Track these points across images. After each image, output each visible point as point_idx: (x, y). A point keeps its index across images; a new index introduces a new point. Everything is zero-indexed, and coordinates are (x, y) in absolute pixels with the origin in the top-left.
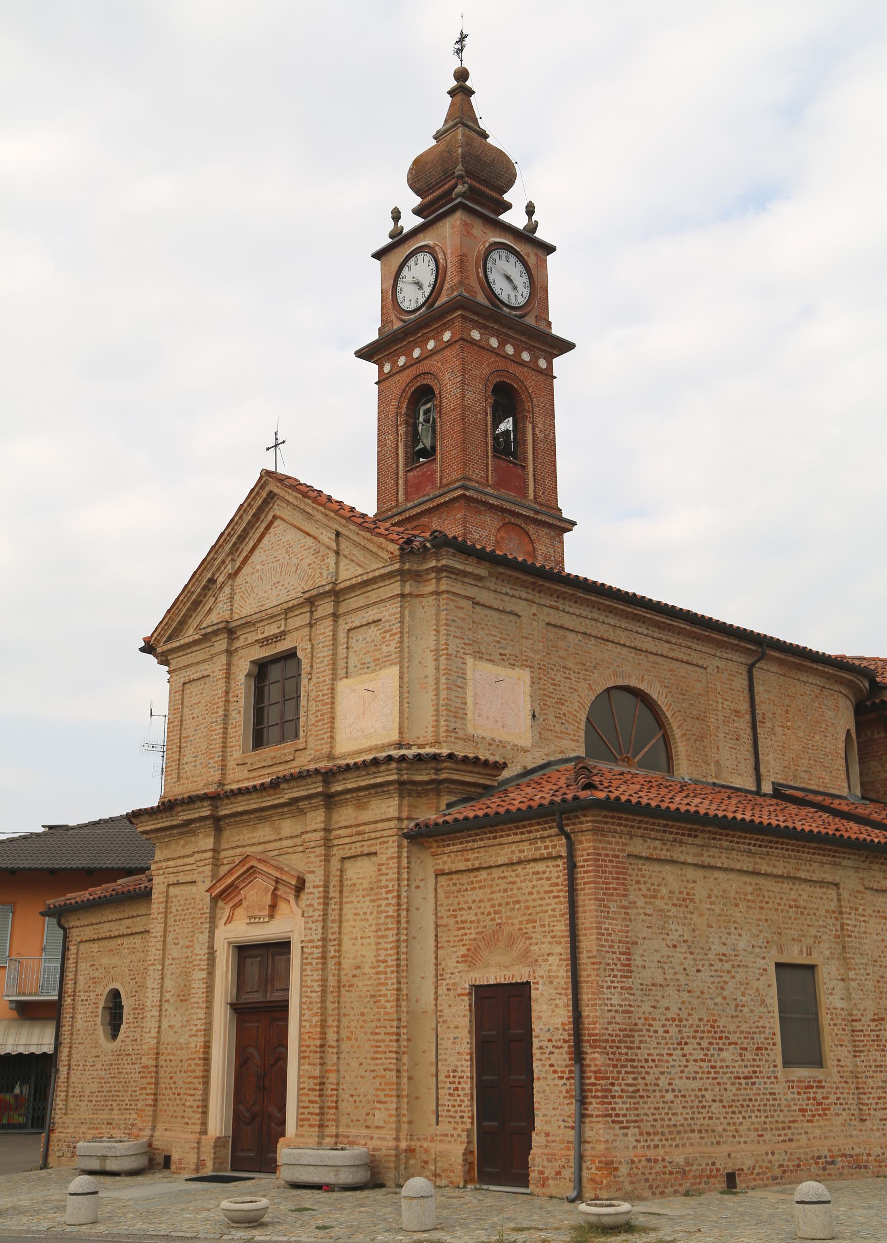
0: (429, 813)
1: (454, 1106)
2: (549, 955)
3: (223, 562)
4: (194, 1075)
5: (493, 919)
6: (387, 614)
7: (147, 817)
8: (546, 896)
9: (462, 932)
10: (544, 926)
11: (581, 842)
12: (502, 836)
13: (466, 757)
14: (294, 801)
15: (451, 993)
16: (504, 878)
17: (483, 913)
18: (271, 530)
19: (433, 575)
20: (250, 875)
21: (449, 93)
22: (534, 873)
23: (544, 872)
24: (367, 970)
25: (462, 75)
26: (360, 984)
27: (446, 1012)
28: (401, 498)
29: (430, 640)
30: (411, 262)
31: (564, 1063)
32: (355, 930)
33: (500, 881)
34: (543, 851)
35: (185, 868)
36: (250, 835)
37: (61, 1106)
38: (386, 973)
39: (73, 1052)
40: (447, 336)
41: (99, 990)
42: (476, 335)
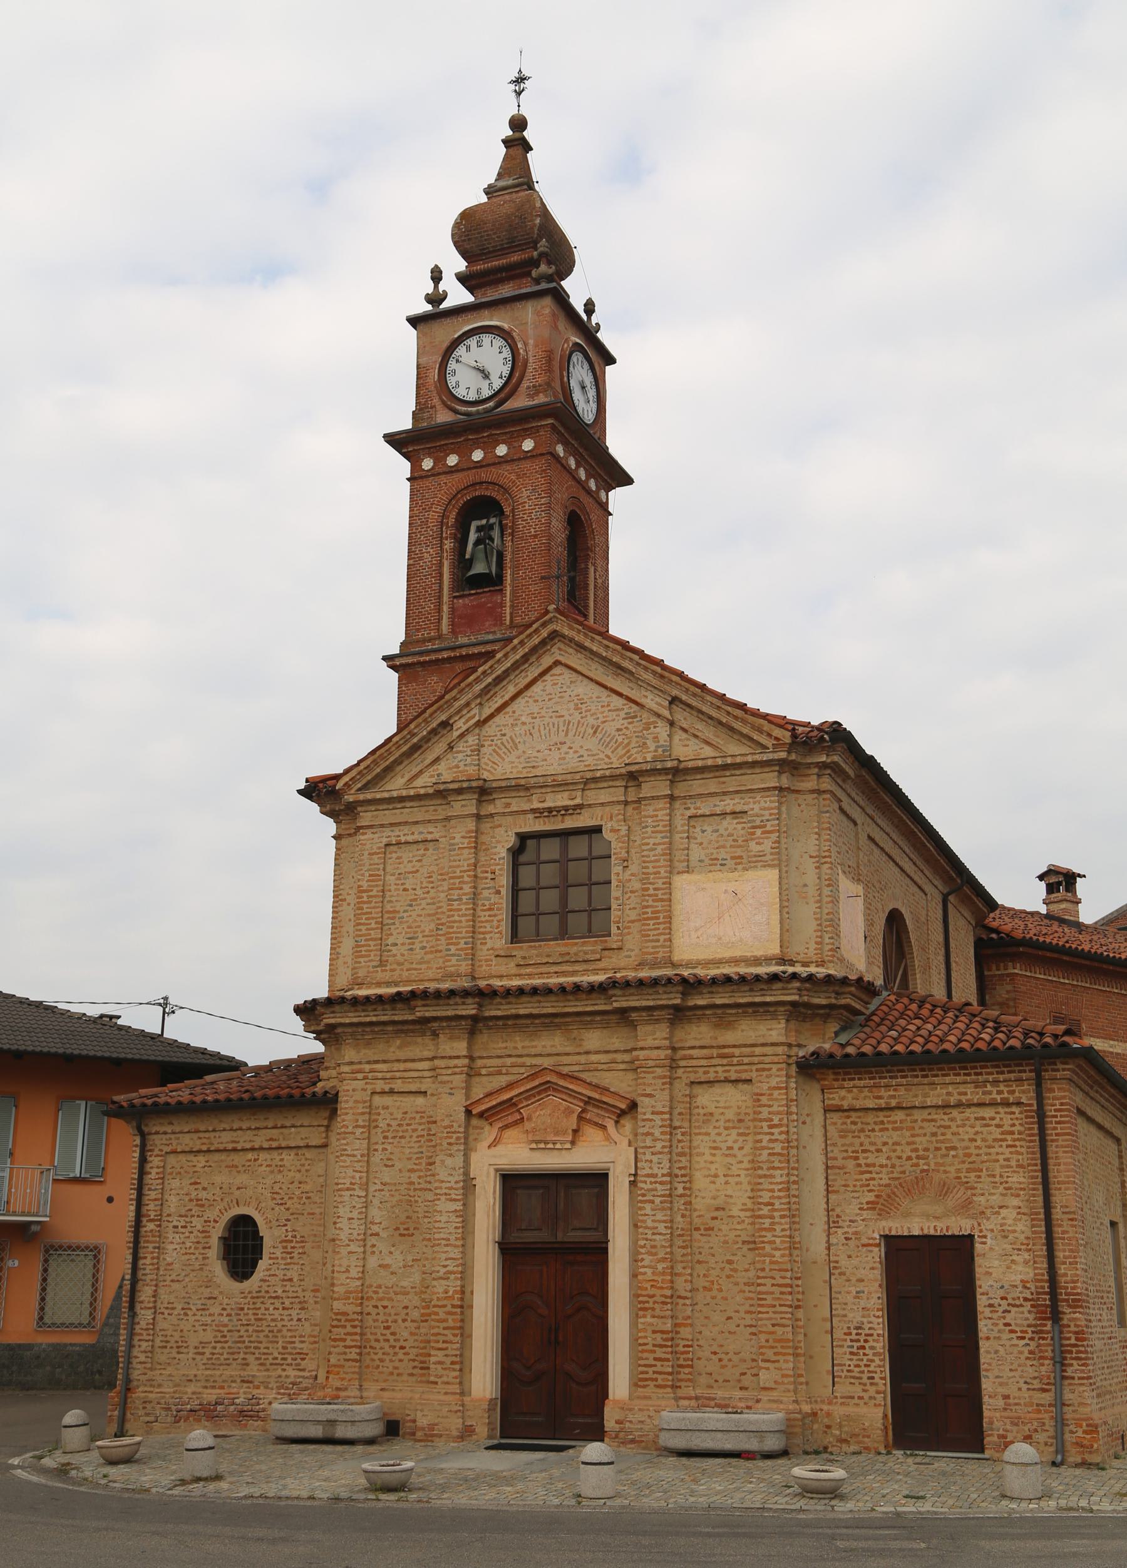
0: (822, 1041)
2: (1001, 1207)
3: (468, 704)
4: (445, 1325)
5: (917, 1165)
6: (756, 807)
8: (996, 1144)
9: (868, 1176)
10: (994, 1176)
11: (1052, 1090)
12: (937, 1076)
13: (846, 978)
14: (623, 1012)
15: (852, 1243)
16: (933, 1120)
17: (900, 1158)
18: (547, 677)
19: (816, 770)
20: (539, 1093)
21: (504, 141)
22: (976, 1119)
23: (993, 1119)
24: (735, 1212)
25: (518, 124)
26: (724, 1227)
27: (844, 1262)
29: (811, 844)
30: (472, 342)
31: (1025, 1323)
32: (713, 1167)
33: (926, 1124)
34: (994, 1096)
35: (406, 1075)
36: (527, 1043)
37: (142, 1358)
38: (772, 1217)
39: (161, 1291)
40: (528, 445)
41: (211, 1214)
42: (560, 450)
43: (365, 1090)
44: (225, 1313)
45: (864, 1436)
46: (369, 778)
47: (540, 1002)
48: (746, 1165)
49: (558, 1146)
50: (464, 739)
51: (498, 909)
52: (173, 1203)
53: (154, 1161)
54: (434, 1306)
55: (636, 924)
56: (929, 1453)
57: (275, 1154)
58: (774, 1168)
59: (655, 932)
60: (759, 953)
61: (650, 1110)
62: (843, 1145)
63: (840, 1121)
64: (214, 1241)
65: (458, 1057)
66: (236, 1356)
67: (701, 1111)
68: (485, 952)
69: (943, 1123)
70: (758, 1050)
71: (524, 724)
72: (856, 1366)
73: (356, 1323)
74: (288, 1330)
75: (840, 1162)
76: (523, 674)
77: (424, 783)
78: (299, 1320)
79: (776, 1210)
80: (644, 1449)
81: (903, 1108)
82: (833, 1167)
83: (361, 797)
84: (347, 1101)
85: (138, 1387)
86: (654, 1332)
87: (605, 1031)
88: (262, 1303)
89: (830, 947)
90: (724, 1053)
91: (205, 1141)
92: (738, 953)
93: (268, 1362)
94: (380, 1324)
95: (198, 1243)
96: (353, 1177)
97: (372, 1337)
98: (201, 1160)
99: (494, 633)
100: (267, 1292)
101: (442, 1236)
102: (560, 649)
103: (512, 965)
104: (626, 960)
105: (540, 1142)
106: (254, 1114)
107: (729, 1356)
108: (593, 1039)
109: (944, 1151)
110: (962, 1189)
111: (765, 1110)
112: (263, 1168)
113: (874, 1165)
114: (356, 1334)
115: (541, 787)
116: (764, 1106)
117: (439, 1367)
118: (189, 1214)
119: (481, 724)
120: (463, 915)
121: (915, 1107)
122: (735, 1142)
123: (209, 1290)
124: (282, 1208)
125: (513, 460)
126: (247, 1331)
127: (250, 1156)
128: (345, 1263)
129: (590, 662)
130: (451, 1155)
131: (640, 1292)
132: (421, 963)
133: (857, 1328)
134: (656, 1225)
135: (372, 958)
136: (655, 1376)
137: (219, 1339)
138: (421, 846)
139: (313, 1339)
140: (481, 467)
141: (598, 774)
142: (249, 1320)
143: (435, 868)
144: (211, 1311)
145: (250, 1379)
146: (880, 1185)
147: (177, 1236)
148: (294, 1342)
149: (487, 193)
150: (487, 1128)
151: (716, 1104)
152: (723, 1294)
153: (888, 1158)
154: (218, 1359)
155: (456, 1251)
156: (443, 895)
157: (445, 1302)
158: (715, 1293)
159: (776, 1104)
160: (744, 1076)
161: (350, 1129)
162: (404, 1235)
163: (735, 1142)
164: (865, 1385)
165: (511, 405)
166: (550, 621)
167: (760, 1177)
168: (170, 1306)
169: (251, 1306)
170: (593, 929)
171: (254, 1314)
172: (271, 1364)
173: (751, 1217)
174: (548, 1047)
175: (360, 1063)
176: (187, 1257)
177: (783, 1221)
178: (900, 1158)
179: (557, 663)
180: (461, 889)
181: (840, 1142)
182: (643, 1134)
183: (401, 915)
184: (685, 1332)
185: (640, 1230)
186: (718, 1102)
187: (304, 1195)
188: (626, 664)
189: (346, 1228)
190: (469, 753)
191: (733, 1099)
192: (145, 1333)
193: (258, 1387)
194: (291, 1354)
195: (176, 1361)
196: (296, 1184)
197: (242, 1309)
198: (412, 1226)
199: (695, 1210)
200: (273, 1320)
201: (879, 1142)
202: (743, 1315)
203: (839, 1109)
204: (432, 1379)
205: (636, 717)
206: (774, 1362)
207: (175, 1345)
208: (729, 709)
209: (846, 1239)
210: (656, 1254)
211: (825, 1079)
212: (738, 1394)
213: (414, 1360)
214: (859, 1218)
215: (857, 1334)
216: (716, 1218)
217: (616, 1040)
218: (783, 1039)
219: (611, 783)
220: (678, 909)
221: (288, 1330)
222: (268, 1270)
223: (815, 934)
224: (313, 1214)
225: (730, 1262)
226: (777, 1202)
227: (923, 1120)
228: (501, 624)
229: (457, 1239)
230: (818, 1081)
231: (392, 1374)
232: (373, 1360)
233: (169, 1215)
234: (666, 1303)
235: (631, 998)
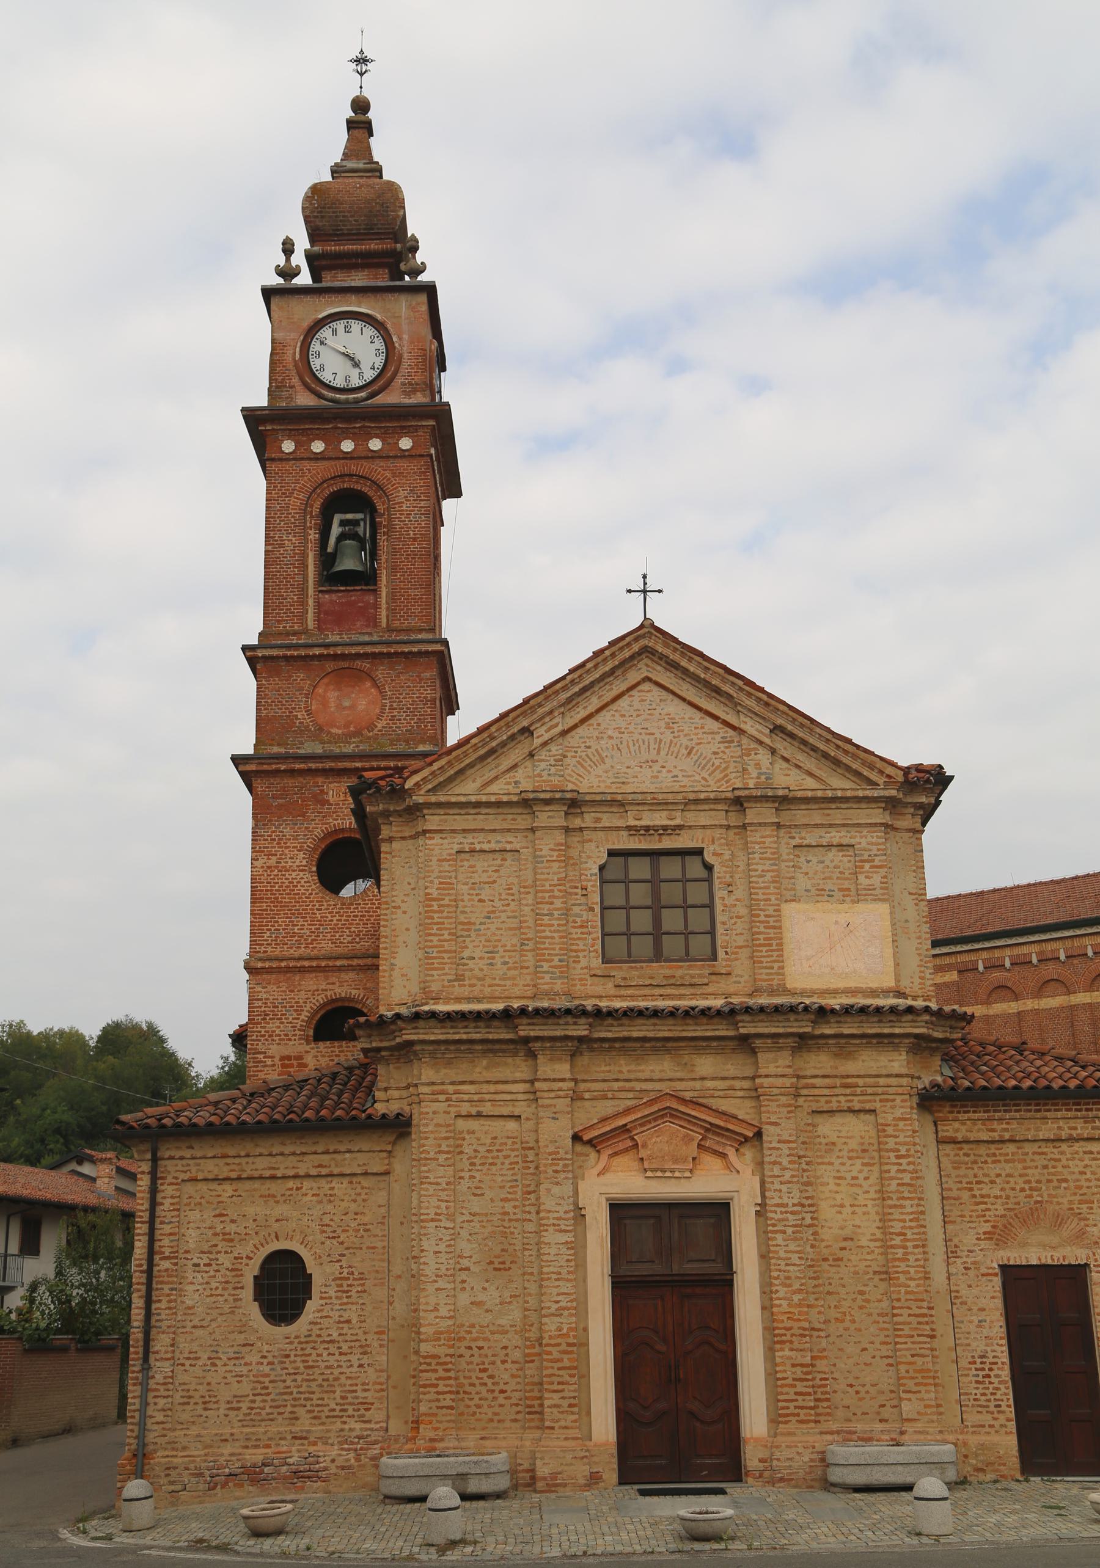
1: (984, 1394)
3: (551, 712)
4: (560, 1365)
5: (1031, 1196)
6: (863, 841)
9: (983, 1207)
12: (1049, 1110)
15: (971, 1273)
16: (1043, 1153)
17: (1013, 1189)
19: (912, 810)
20: (655, 1120)
22: (1085, 1153)
24: (864, 1242)
25: (361, 106)
26: (853, 1258)
27: (964, 1292)
28: (311, 623)
30: (340, 325)
32: (838, 1197)
33: (1036, 1157)
36: (633, 1067)
37: (160, 1417)
38: (905, 1247)
39: (180, 1339)
41: (243, 1250)
43: (449, 1113)
44: (265, 1361)
45: (1000, 1465)
46: (442, 779)
47: (655, 1025)
48: (872, 1195)
49: (677, 1174)
50: (547, 748)
51: (593, 927)
52: (192, 1238)
53: (167, 1191)
54: (547, 1345)
55: (744, 950)
56: (1066, 1479)
57: (323, 1182)
58: (903, 1198)
59: (769, 959)
60: (874, 985)
61: (776, 1138)
62: (957, 1176)
63: (952, 1153)
64: (249, 1281)
65: (563, 1080)
66: (281, 1410)
67: (823, 1141)
68: (579, 971)
69: (1052, 1156)
70: (882, 1081)
71: (611, 738)
72: (982, 1395)
73: (450, 1366)
74: (348, 1378)
75: (955, 1193)
76: (607, 687)
77: (501, 789)
78: (361, 1366)
79: (908, 1240)
80: (795, 1487)
81: (1015, 1141)
82: (948, 1198)
83: (433, 799)
84: (427, 1125)
85: (155, 1451)
86: (793, 1365)
87: (718, 1057)
88: (313, 1348)
89: (931, 982)
90: (847, 1083)
92: (852, 984)
93: (323, 1415)
94: (474, 1366)
95: (227, 1282)
96: (438, 1207)
97: (466, 1382)
98: (228, 1189)
99: (370, 634)
100: (319, 1336)
101: (552, 1269)
102: (647, 665)
103: (610, 985)
104: (731, 987)
105: (656, 1170)
107: (866, 1388)
108: (705, 1064)
109: (1055, 1183)
110: (1076, 1220)
111: (891, 1141)
112: (309, 1198)
113: (989, 1196)
114: (450, 1378)
115: (639, 804)
116: (891, 1136)
117: (555, 1410)
118: (214, 1250)
119: (564, 733)
120: (555, 931)
121: (1028, 1140)
122: (861, 1171)
123: (243, 1336)
124: (335, 1242)
125: (388, 457)
126: (295, 1380)
127: (291, 1184)
128: (432, 1300)
129: (681, 682)
130: (557, 1183)
131: (775, 1325)
132: (504, 979)
133: (981, 1357)
134: (789, 1255)
135: (447, 971)
136: (797, 1411)
137: (259, 1391)
138: (497, 855)
139: (378, 1387)
140: (352, 458)
141: (702, 796)
142: (298, 1368)
143: (515, 881)
144: (247, 1360)
145: (304, 1434)
146: (995, 1216)
147: (199, 1275)
148: (356, 1391)
149: (333, 172)
150: (593, 1155)
151: (837, 1134)
152: (856, 1325)
153: (1002, 1189)
155: (569, 1285)
156: (527, 909)
157: (559, 1340)
158: (847, 1324)
159: (902, 1135)
160: (868, 1106)
161: (432, 1155)
162: (500, 1269)
163: (861, 1171)
164: (992, 1413)
165: (380, 399)
166: (643, 636)
167: (890, 1207)
168: (192, 1356)
169: (299, 1353)
170: (634, 953)
171: (303, 1361)
172: (327, 1417)
173: (881, 1247)
174: (658, 1072)
175: (443, 1083)
176: (213, 1299)
177: (916, 1251)
178: (1013, 1189)
179: (647, 679)
180: (552, 903)
181: (954, 1173)
182: (770, 1163)
183: (477, 927)
184: (821, 1365)
185: (773, 1261)
186: (840, 1131)
187: (362, 1228)
188: (726, 688)
189: (432, 1263)
190: (553, 763)
191: (857, 1129)
192: (162, 1388)
193: (315, 1444)
195: (203, 1419)
196: (351, 1215)
197: (288, 1356)
198: (507, 1259)
199: (822, 1240)
200: (327, 1367)
201: (992, 1173)
202: (879, 1347)
203: (953, 1141)
204: (547, 1424)
205: (732, 742)
206: (915, 1392)
207: (200, 1401)
208: (840, 743)
209: (966, 1268)
210: (790, 1286)
211: (939, 1111)
212: (879, 1426)
213: (517, 1405)
214: (976, 1248)
215: (982, 1363)
216: (845, 1249)
217: (734, 1066)
218: (904, 1071)
219: (712, 806)
220: (788, 936)
221: (348, 1378)
222: (319, 1311)
223: (918, 969)
224: (374, 1248)
225: (862, 1293)
226: (909, 1232)
227: (1034, 1153)
228: (376, 626)
229: (569, 1273)
230: (931, 1112)
231: (491, 1420)
232: (469, 1406)
233: (187, 1252)
234: (805, 1336)
235: (760, 1024)
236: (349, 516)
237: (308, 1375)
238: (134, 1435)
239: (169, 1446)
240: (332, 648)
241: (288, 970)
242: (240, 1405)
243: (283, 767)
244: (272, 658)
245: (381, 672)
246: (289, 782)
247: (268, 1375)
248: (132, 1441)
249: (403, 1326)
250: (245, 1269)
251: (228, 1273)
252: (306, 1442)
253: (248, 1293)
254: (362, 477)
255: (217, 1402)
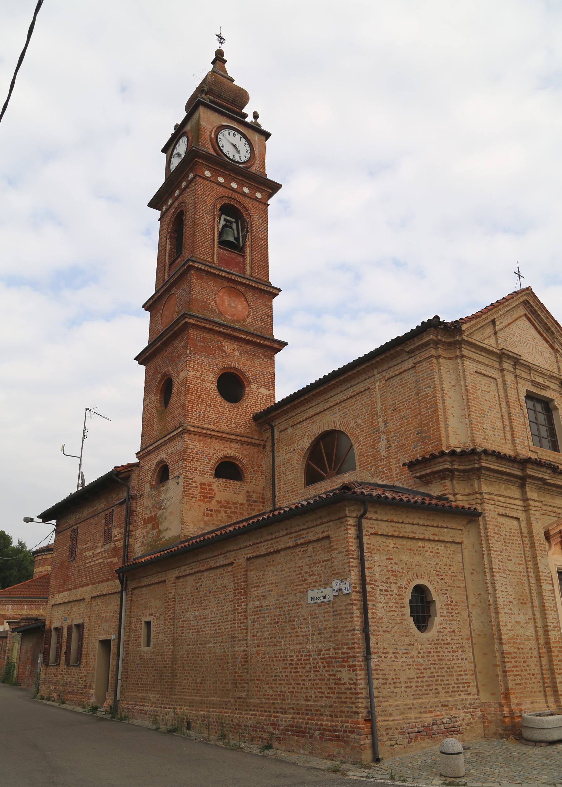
7: (494, 459)
30: (232, 132)
44: (420, 655)
66: (431, 688)
74: (458, 667)
78: (462, 659)
91: (397, 529)
95: (397, 603)
98: (391, 542)
100: (442, 640)
106: (429, 516)
112: (428, 553)
123: (408, 638)
124: (443, 581)
126: (435, 668)
127: (420, 543)
137: (419, 675)
145: (446, 703)
147: (383, 597)
154: (421, 690)
168: (385, 651)
169: (435, 650)
176: (391, 613)
187: (453, 574)
194: (461, 683)
195: (394, 694)
221: (458, 667)
236: (229, 218)
237: (440, 665)
238: (364, 706)
239: (383, 714)
240: (230, 275)
241: (206, 435)
242: (412, 684)
243: (208, 326)
244: (201, 269)
245: (249, 295)
246: (207, 335)
247: (422, 665)
248: (362, 710)
249: (480, 635)
250: (404, 594)
251: (397, 597)
252: (447, 708)
253: (407, 611)
254: (239, 202)
255: (400, 683)
